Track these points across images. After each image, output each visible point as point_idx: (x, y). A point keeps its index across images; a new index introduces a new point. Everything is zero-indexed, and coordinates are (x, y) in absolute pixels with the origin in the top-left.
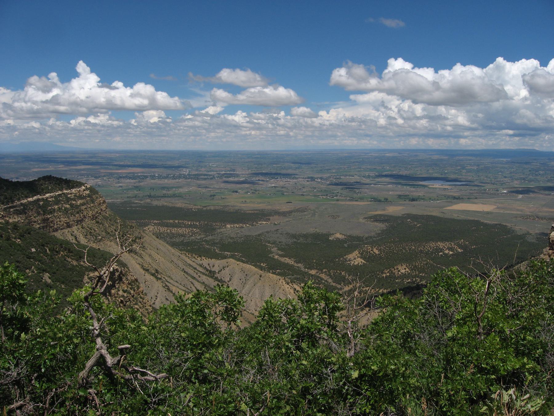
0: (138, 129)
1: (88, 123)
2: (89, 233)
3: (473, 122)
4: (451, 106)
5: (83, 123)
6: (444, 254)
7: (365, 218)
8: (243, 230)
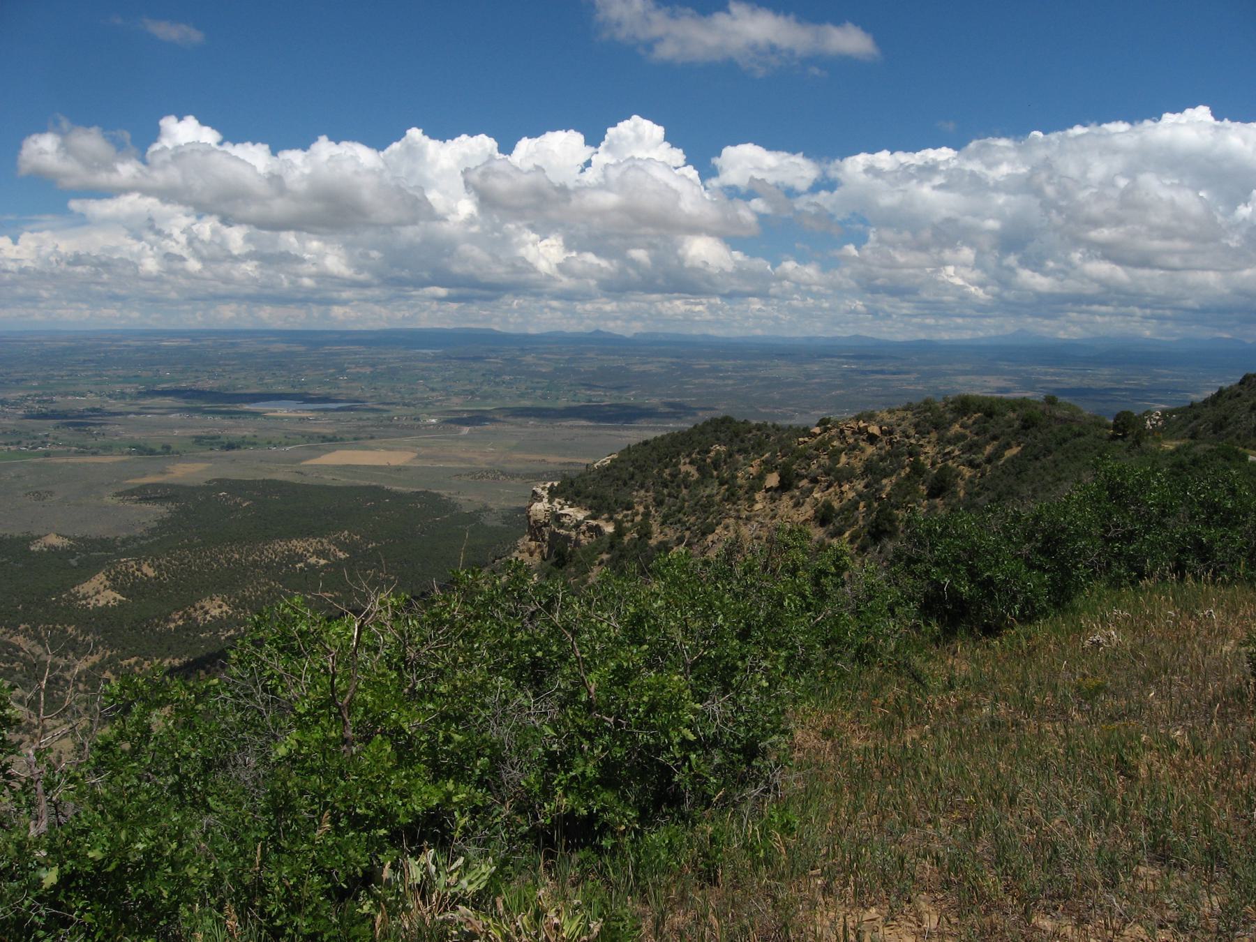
3: (360, 268)
4: (309, 232)
6: (307, 565)
7: (118, 494)
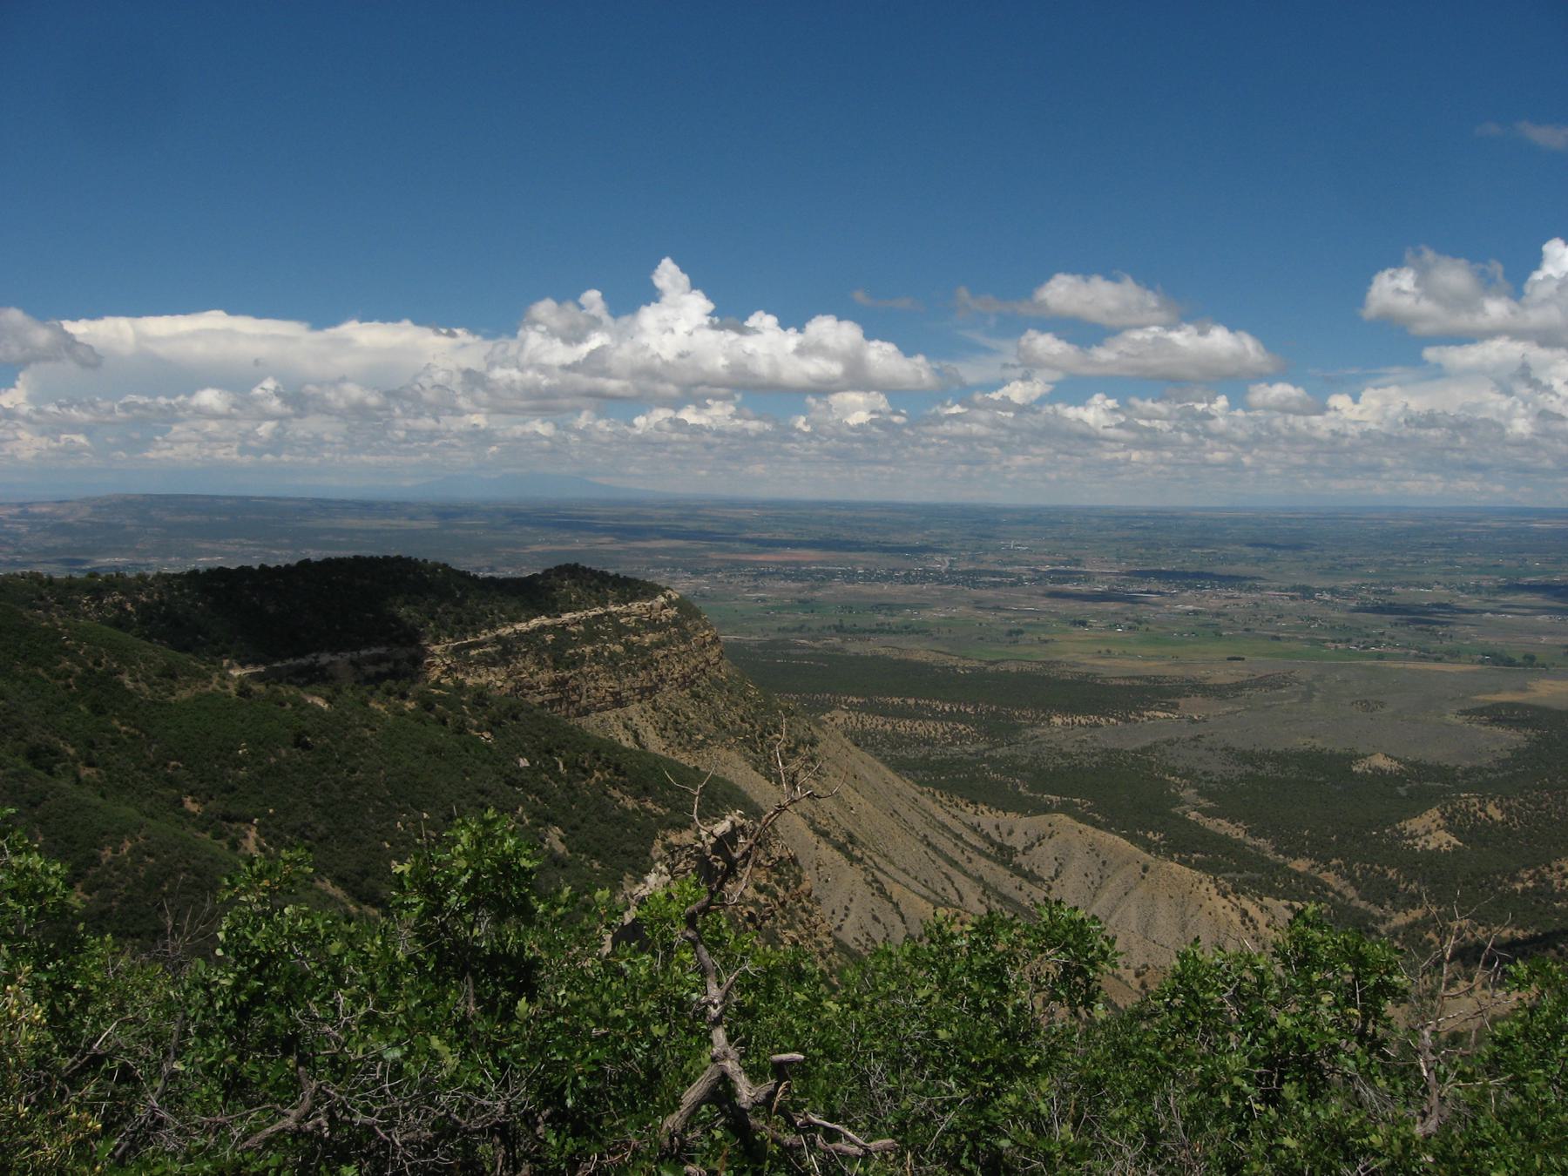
0: (814, 444)
1: (680, 425)
2: (673, 726)
5: (667, 426)
8: (1098, 733)
